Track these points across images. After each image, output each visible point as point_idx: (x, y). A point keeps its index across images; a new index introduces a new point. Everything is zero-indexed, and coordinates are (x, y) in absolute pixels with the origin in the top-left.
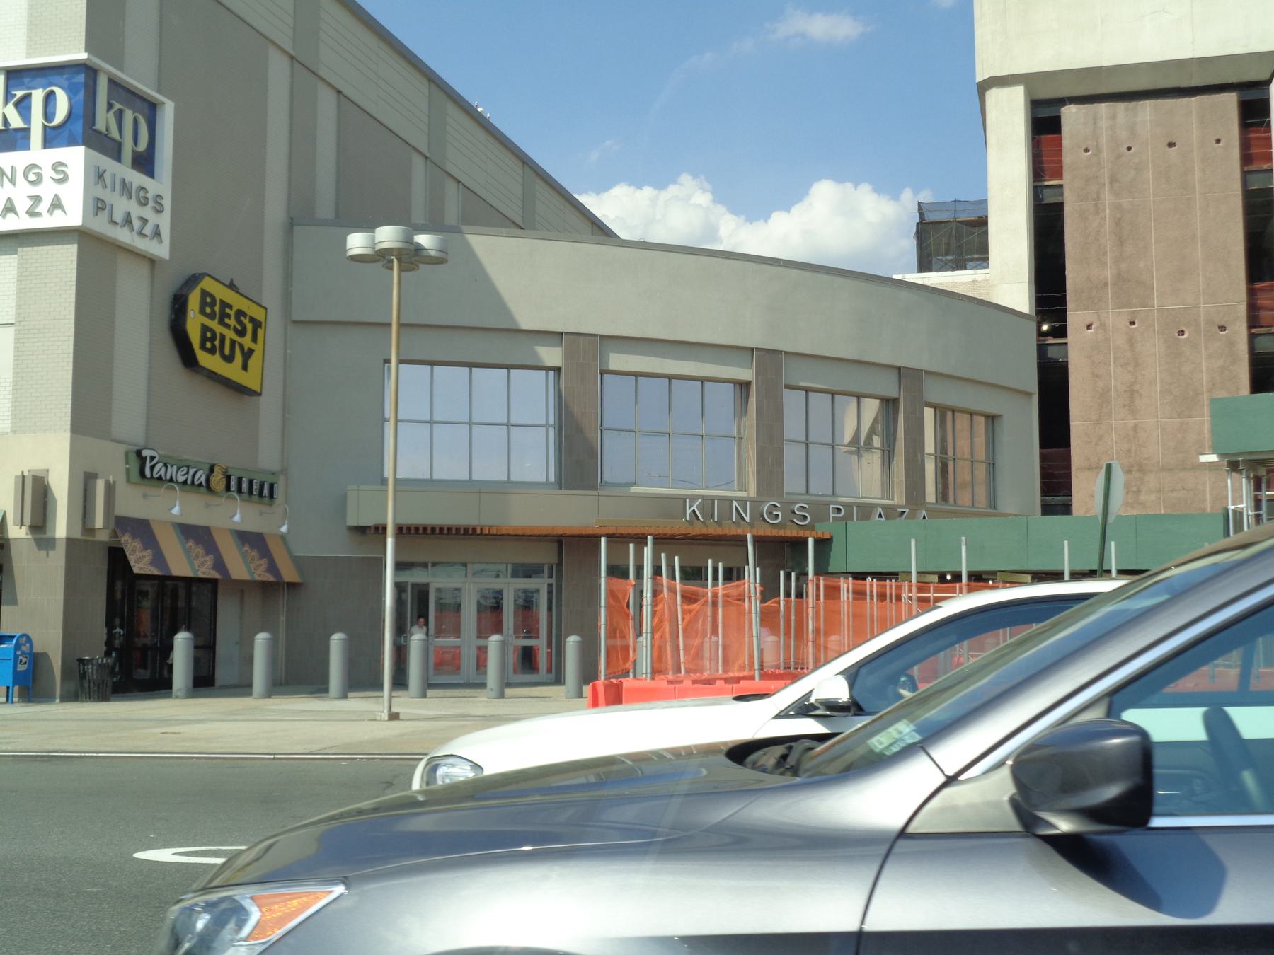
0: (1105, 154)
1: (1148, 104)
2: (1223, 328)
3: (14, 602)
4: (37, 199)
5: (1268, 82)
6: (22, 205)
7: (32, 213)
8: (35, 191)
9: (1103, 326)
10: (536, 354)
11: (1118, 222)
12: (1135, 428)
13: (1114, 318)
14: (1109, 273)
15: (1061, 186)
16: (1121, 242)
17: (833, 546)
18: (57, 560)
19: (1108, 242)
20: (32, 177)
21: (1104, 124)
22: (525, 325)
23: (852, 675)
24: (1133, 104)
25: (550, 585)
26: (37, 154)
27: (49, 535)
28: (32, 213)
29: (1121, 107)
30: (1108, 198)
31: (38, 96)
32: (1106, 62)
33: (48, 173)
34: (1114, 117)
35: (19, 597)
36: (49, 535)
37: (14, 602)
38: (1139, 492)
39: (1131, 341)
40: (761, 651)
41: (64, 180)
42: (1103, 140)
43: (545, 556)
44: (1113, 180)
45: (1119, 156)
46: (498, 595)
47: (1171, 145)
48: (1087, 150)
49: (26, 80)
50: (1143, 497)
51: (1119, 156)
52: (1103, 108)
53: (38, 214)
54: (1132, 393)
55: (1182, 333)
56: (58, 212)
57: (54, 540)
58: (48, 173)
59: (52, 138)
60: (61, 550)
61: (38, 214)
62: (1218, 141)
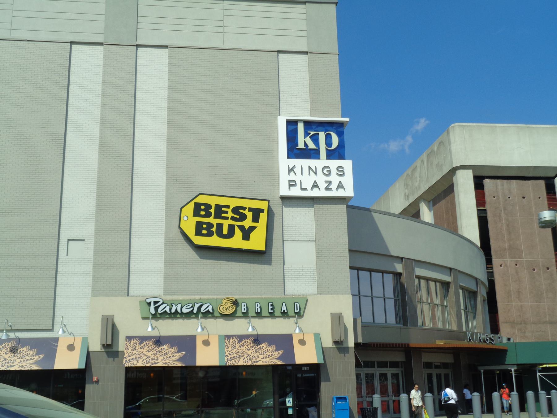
0: (501, 199)
1: (514, 182)
2: (548, 268)
3: (329, 380)
4: (330, 183)
5: (555, 177)
6: (323, 185)
7: (327, 189)
8: (328, 179)
9: (506, 265)
10: (394, 267)
11: (508, 225)
12: (521, 306)
13: (510, 262)
14: (506, 245)
15: (486, 210)
16: (510, 233)
17: (508, 353)
18: (351, 358)
19: (505, 233)
20: (325, 171)
21: (500, 187)
22: (393, 254)
23: (376, 409)
24: (509, 181)
25: (402, 371)
26: (322, 162)
27: (345, 345)
28: (327, 189)
29: (505, 182)
30: (503, 216)
31: (322, 135)
32: (502, 164)
33: (334, 171)
34: (503, 185)
35: (331, 378)
36: (345, 345)
37: (329, 380)
38: (525, 332)
39: (517, 272)
40: (537, 399)
41: (343, 175)
42: (500, 194)
43: (400, 357)
44: (505, 209)
45: (506, 200)
46: (440, 375)
47: (524, 198)
48: (494, 197)
49: (314, 127)
50: (527, 334)
51: (506, 200)
52: (499, 181)
53: (331, 190)
54: (519, 293)
55: (534, 269)
56: (340, 190)
57: (348, 348)
58: (334, 171)
59: (331, 155)
60: (352, 353)
61: (331, 190)
62: (540, 198)
